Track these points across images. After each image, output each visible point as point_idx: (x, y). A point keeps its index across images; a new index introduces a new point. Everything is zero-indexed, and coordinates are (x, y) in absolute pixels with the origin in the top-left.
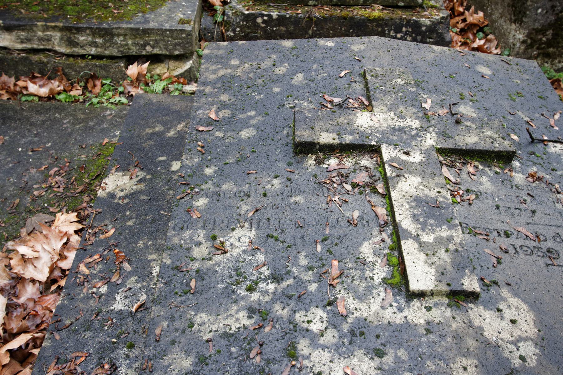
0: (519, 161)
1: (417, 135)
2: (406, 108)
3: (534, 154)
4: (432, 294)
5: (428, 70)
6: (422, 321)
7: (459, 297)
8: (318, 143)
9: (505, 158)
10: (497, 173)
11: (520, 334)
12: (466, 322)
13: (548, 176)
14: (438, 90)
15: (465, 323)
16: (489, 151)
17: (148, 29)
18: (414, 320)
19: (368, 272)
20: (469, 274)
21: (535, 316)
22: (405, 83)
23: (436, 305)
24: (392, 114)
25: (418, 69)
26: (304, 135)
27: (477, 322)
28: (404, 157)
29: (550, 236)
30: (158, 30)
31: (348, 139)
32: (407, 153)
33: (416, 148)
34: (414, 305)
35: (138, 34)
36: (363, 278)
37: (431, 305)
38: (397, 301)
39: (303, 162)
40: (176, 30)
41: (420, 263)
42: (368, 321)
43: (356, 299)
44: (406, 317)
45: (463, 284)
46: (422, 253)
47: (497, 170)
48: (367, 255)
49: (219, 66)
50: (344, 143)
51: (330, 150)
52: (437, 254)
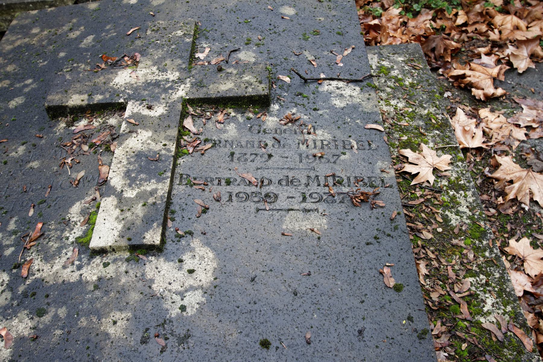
0: (280, 103)
1: (171, 88)
2: (172, 60)
3: (301, 94)
4: (113, 250)
5: (224, 17)
6: (95, 278)
7: (139, 250)
8: (67, 106)
9: (262, 103)
10: (249, 119)
11: (192, 284)
12: (138, 275)
13: (305, 117)
14: (224, 38)
15: (136, 276)
16: (240, 97)
17: (11, 4)
18: (88, 277)
19: (67, 232)
20: (155, 227)
21: (218, 265)
22: (185, 34)
23: (115, 261)
24: (154, 69)
25: (213, 18)
26: (54, 99)
27: (149, 275)
28: (146, 112)
29: (275, 180)
30: (20, 4)
31: (98, 98)
32: (150, 108)
33: (164, 101)
34: (94, 263)
35: (3, 10)
36: (60, 238)
37: (110, 261)
38: (80, 260)
39: (55, 126)
40: (38, 2)
41: (111, 220)
42: (45, 281)
43: (43, 261)
44: (81, 275)
45: (144, 238)
46: (118, 209)
47: (251, 115)
48: (73, 215)
49: (20, 36)
50: (91, 103)
51: (78, 112)
52: (133, 210)
